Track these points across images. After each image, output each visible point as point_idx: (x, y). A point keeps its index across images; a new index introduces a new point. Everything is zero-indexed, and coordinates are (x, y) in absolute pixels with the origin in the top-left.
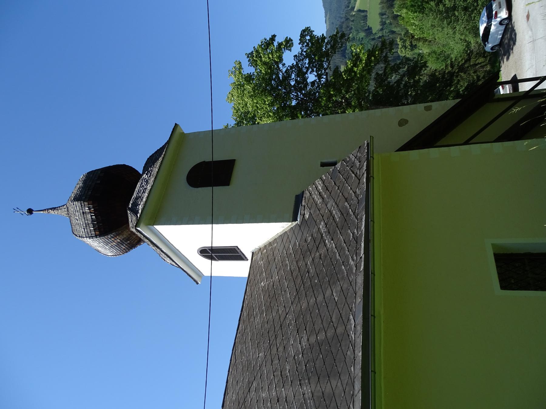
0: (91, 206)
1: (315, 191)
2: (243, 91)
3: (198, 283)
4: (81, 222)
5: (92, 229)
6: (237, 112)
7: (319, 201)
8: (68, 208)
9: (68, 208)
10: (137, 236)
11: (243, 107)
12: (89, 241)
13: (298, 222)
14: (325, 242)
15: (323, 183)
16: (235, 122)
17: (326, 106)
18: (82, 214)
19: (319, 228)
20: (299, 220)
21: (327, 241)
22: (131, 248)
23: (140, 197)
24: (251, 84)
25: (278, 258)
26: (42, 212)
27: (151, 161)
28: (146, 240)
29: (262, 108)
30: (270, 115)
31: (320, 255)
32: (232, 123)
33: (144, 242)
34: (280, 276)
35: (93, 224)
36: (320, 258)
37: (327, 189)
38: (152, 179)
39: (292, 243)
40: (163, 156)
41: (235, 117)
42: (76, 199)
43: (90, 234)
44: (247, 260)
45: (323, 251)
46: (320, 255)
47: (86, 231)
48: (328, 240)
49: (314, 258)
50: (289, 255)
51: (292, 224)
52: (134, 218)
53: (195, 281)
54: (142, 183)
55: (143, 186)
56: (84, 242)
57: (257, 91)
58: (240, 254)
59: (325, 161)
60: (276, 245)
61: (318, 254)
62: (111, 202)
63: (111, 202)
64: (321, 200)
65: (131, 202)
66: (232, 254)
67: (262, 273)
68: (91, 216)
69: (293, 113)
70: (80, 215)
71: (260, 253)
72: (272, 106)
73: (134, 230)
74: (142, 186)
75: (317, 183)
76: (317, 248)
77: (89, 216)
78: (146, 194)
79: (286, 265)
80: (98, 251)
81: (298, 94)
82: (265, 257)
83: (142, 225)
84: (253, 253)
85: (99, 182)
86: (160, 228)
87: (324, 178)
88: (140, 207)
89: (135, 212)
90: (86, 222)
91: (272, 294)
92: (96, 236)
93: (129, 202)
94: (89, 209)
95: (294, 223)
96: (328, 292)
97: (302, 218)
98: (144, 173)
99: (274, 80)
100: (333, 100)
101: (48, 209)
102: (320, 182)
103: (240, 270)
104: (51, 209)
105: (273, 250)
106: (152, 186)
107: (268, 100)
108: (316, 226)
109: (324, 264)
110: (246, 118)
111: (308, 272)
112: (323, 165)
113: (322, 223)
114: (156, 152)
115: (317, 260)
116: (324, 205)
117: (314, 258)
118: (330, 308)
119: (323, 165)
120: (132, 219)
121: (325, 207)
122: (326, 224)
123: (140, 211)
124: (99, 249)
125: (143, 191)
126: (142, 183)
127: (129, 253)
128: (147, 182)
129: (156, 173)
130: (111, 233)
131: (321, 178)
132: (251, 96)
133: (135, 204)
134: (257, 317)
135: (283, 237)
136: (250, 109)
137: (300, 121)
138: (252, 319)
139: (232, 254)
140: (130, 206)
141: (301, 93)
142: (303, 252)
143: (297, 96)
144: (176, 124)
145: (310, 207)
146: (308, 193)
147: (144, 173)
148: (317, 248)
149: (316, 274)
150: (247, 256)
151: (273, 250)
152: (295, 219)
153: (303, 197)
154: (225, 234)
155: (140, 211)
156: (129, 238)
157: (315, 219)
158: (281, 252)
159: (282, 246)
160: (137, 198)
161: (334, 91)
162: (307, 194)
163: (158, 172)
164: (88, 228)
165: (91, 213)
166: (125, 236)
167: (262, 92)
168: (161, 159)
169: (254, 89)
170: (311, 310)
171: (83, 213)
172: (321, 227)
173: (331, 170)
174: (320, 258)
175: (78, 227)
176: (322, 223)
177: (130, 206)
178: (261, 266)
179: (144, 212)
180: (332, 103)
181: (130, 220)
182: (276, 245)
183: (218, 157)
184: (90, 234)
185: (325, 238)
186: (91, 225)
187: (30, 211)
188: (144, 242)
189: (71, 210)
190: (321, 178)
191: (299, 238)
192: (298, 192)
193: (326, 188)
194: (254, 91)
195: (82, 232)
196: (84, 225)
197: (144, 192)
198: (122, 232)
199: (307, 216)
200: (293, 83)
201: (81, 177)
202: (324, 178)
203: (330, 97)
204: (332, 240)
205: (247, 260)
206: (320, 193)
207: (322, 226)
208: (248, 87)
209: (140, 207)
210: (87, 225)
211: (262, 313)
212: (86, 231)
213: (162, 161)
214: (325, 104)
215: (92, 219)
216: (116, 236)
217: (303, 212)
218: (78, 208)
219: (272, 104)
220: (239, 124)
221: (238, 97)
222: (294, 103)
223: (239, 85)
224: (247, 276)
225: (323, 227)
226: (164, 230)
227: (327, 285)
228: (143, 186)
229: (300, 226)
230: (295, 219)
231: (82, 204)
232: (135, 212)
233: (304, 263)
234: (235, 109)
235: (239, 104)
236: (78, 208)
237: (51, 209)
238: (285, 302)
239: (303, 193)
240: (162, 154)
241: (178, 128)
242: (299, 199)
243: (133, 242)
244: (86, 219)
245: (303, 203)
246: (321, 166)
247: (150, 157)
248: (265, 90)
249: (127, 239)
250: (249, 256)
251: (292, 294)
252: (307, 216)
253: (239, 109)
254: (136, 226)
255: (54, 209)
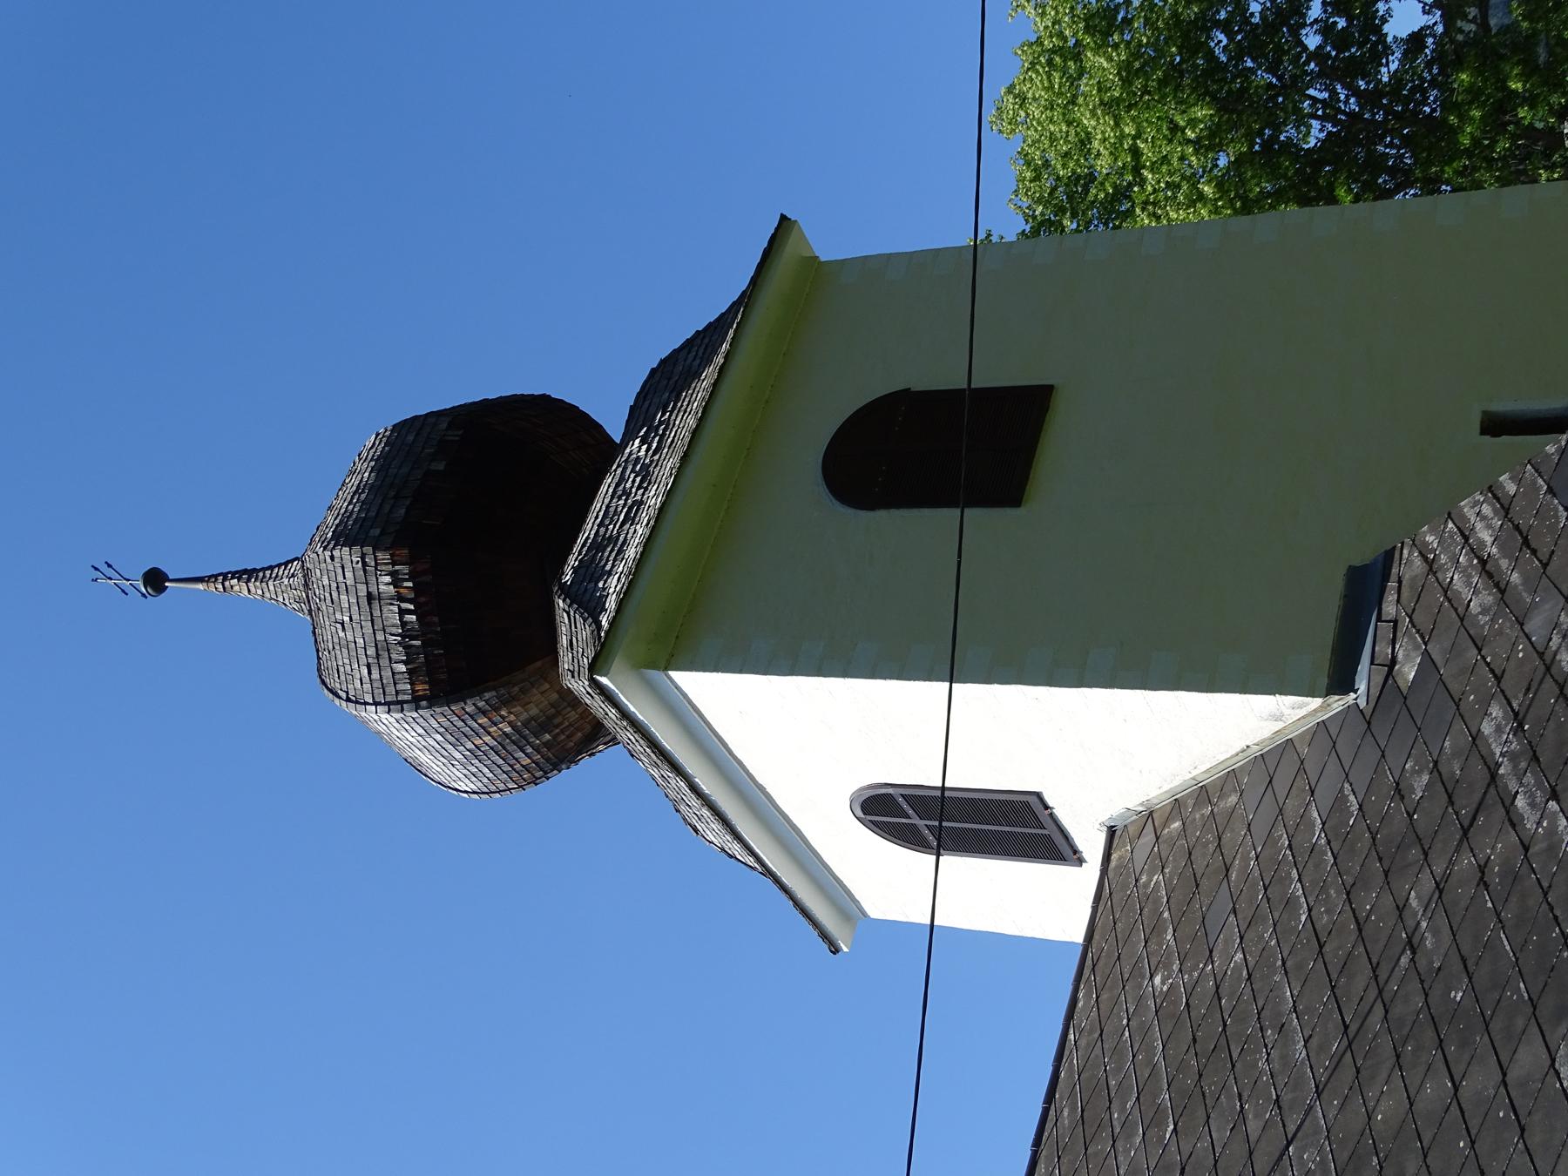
0: (404, 569)
1: (1460, 546)
2: (1074, 81)
3: (835, 950)
4: (359, 636)
5: (402, 668)
6: (1037, 178)
7: (1480, 601)
8: (307, 574)
9: (307, 574)
10: (586, 712)
11: (1067, 155)
12: (385, 721)
13: (1360, 695)
14: (1508, 806)
15: (1505, 509)
16: (1022, 225)
17: (1479, 152)
18: (364, 602)
19: (1476, 736)
20: (1362, 687)
21: (1520, 802)
22: (557, 767)
23: (613, 540)
24: (1116, 46)
25: (1245, 863)
26: (201, 586)
27: (667, 381)
28: (627, 735)
29: (1165, 160)
30: (1201, 197)
31: (1482, 869)
32: (1006, 222)
33: (614, 741)
34: (1255, 950)
35: (407, 647)
36: (1483, 883)
37: (1526, 542)
38: (670, 463)
39: (1325, 795)
40: (719, 359)
41: (1026, 202)
42: (345, 536)
43: (391, 690)
44: (1080, 861)
45: (1497, 848)
46: (1482, 869)
47: (375, 675)
48: (1531, 796)
49: (1447, 877)
50: (1303, 856)
51: (1322, 708)
52: (584, 632)
53: (825, 936)
54: (622, 479)
55: (627, 494)
56: (364, 722)
57: (1138, 84)
58: (1050, 830)
59: (1506, 405)
60: (1233, 799)
61: (1467, 861)
62: (491, 559)
63: (487, 553)
64: (1488, 598)
65: (572, 561)
66: (1013, 826)
67: (1157, 929)
68: (402, 612)
69: (1308, 182)
70: (358, 607)
71: (1149, 837)
72: (1209, 149)
73: (579, 686)
74: (620, 492)
75: (1470, 514)
76: (1465, 832)
77: (391, 614)
78: (641, 530)
79: (1290, 902)
80: (418, 768)
81: (1333, 93)
82: (1173, 860)
83: (618, 664)
84: (1112, 832)
85: (441, 466)
86: (696, 685)
87: (1511, 488)
88: (613, 586)
89: (590, 606)
90: (380, 637)
91: (1212, 1040)
92: (416, 701)
93: (564, 561)
94: (396, 583)
95: (1338, 703)
96: (1528, 1058)
97: (1378, 679)
98: (629, 435)
99: (1226, 27)
100: (1518, 122)
101: (225, 576)
102: (1486, 510)
103: (1045, 905)
104: (237, 575)
105: (1219, 826)
106: (669, 494)
107: (1193, 123)
108: (1459, 725)
109: (1507, 915)
110: (1076, 202)
111: (1412, 945)
112: (1495, 425)
113: (1496, 711)
114: (689, 344)
115: (1462, 892)
116: (1505, 624)
117: (1447, 877)
118: (1535, 1138)
119: (1495, 425)
120: (573, 635)
121: (1512, 632)
122: (1518, 718)
123: (611, 603)
124: (424, 758)
125: (627, 517)
126: (622, 479)
127: (545, 785)
128: (646, 474)
129: (685, 435)
130: (480, 694)
131: (1493, 491)
132: (1109, 106)
133: (592, 572)
134: (1130, 1136)
135: (1270, 764)
136: (1103, 165)
137: (1347, 216)
138: (1102, 1146)
139: (1013, 826)
140: (568, 577)
141: (1355, 92)
142: (1385, 848)
143: (1331, 103)
144: (783, 218)
145: (1427, 627)
146: (1418, 562)
147: (629, 435)
148: (1465, 832)
149: (1456, 959)
150: (1080, 844)
151: (1219, 826)
152: (1341, 682)
153: (1386, 577)
154: (1003, 732)
155: (611, 603)
156: (550, 718)
157: (1455, 687)
158: (1260, 831)
159: (1269, 804)
160: (598, 546)
161: (1524, 77)
162: (1410, 565)
163: (695, 433)
164: (384, 662)
165: (401, 598)
166: (534, 711)
167: (1163, 83)
168: (710, 374)
169: (1127, 73)
170: (1427, 1137)
171: (370, 597)
172: (1487, 728)
173: (1551, 449)
174: (1483, 883)
175: (343, 658)
176: (1496, 711)
177: (568, 577)
178: (1150, 898)
179: (629, 609)
180: (1514, 137)
181: (564, 641)
182: (1233, 799)
183: (989, 376)
184: (391, 690)
185: (1513, 786)
186: (399, 654)
187: (156, 580)
188: (614, 741)
189: (321, 580)
190: (1493, 491)
191: (1361, 777)
192: (1363, 554)
193: (1521, 539)
194: (1126, 82)
195: (358, 678)
196: (371, 651)
197: (630, 519)
198: (523, 691)
199: (1408, 671)
200: (1312, 41)
201: (367, 438)
202: (1511, 488)
203: (1504, 104)
204: (1554, 796)
205: (1080, 861)
206: (1483, 562)
207: (1493, 723)
208: (1102, 64)
209: (613, 586)
210: (381, 649)
211: (1154, 1121)
212: (375, 675)
213: (715, 385)
214: (1476, 142)
215: (403, 624)
216: (497, 709)
217: (1384, 650)
218: (349, 575)
219: (1209, 143)
220: (1041, 228)
221: (1051, 107)
222: (1316, 133)
223: (1053, 51)
224: (1078, 936)
225: (1499, 730)
226: (714, 693)
227: (1520, 1023)
228: (627, 494)
229: (1366, 719)
230: (1341, 682)
231: (370, 560)
232: (590, 606)
233: (1388, 901)
234: (1028, 163)
235: (1052, 139)
236: (349, 575)
237: (237, 575)
238: (1281, 1080)
239: (1389, 557)
240: (715, 352)
241: (795, 231)
242: (1364, 588)
243: (566, 736)
244: (378, 625)
245: (1390, 609)
246: (1485, 430)
247: (663, 362)
248: (1173, 77)
249: (541, 725)
250: (1091, 844)
251: (1323, 1047)
252: (1408, 671)
253: (1047, 164)
254: (593, 668)
255: (246, 575)
